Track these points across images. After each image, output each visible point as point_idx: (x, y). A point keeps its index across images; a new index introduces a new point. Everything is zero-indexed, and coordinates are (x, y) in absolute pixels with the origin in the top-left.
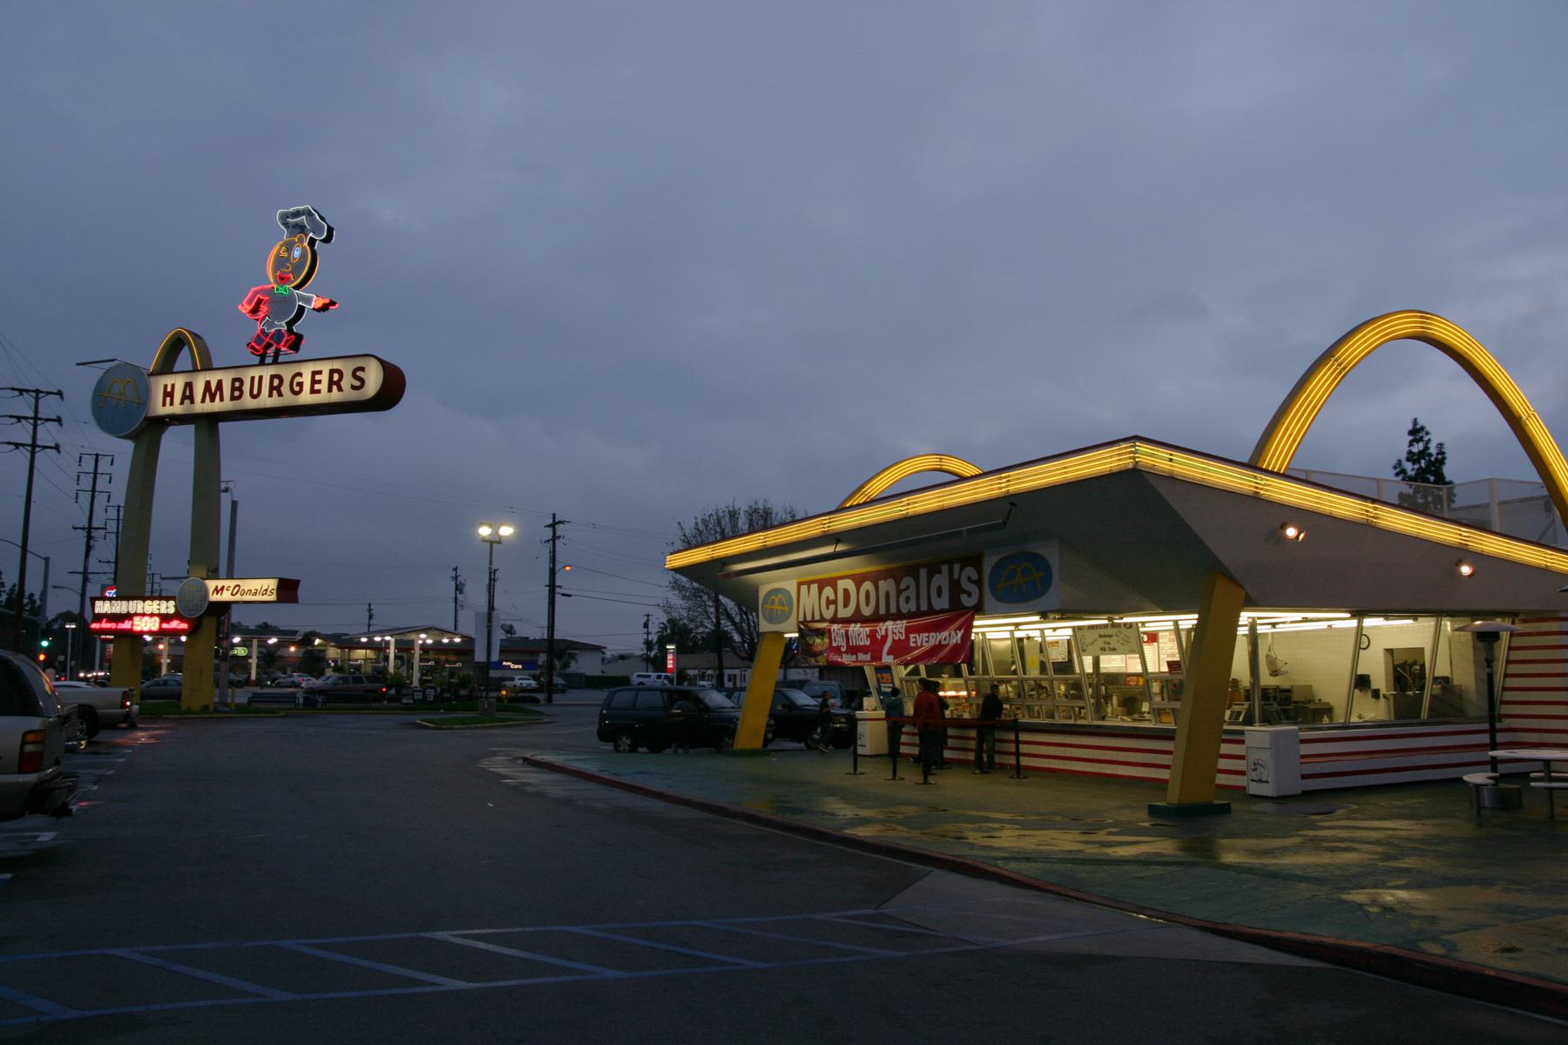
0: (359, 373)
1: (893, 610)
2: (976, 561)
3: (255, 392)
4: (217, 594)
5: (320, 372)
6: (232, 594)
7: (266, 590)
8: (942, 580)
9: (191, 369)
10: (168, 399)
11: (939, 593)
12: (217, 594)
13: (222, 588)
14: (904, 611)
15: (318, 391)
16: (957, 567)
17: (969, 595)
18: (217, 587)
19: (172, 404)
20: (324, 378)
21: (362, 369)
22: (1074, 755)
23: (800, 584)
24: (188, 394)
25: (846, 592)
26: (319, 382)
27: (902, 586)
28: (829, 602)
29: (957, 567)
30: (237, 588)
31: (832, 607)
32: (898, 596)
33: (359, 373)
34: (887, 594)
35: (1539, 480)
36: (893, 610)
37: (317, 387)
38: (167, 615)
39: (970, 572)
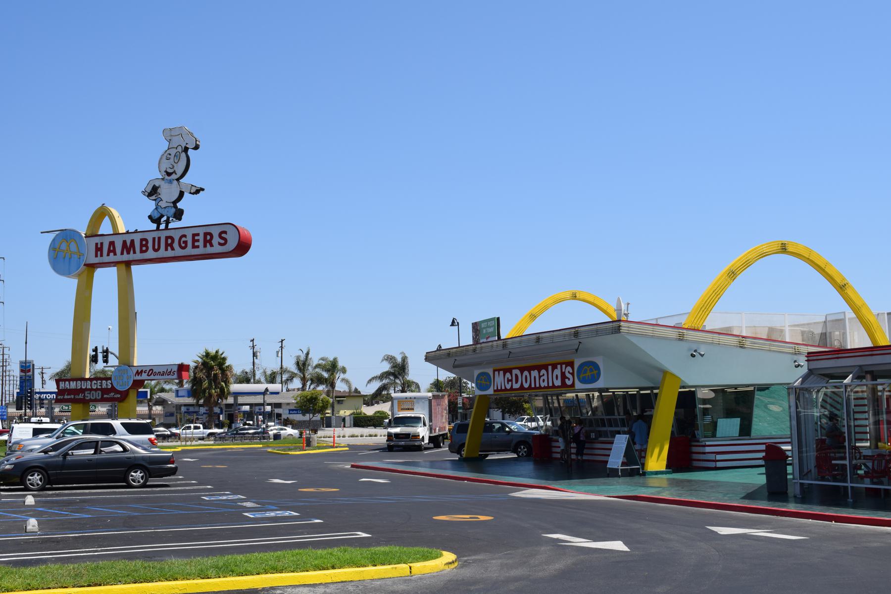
0: (223, 235)
1: (538, 385)
2: (571, 364)
3: (156, 247)
4: (138, 375)
5: (198, 235)
6: (148, 375)
7: (170, 372)
8: (557, 372)
9: (112, 232)
10: (99, 253)
11: (557, 378)
12: (138, 375)
13: (142, 371)
14: (542, 386)
15: (198, 247)
16: (564, 366)
17: (569, 379)
18: (138, 371)
19: (101, 255)
20: (201, 238)
21: (225, 232)
22: (606, 447)
23: (494, 371)
24: (112, 249)
25: (517, 376)
26: (198, 241)
27: (541, 374)
28: (509, 381)
29: (564, 366)
30: (151, 371)
31: (510, 383)
32: (539, 379)
33: (223, 235)
34: (535, 377)
35: (855, 316)
36: (538, 385)
37: (196, 244)
38: (107, 389)
39: (569, 369)
